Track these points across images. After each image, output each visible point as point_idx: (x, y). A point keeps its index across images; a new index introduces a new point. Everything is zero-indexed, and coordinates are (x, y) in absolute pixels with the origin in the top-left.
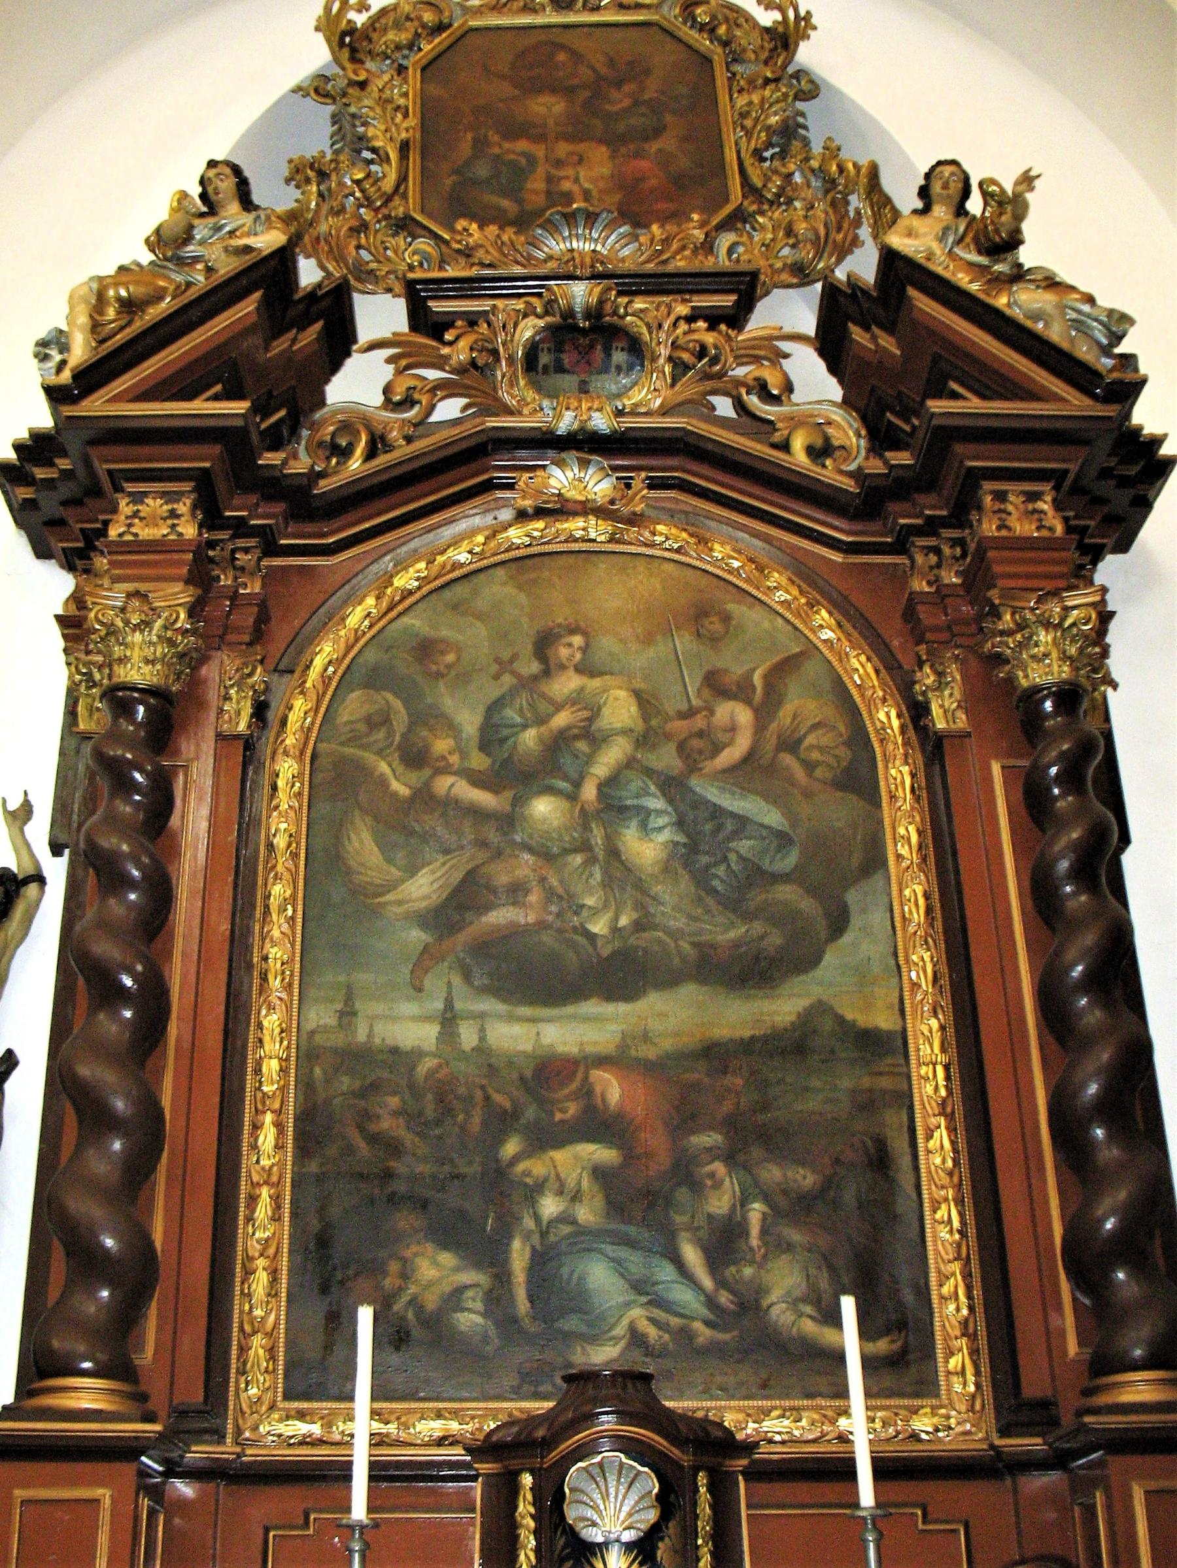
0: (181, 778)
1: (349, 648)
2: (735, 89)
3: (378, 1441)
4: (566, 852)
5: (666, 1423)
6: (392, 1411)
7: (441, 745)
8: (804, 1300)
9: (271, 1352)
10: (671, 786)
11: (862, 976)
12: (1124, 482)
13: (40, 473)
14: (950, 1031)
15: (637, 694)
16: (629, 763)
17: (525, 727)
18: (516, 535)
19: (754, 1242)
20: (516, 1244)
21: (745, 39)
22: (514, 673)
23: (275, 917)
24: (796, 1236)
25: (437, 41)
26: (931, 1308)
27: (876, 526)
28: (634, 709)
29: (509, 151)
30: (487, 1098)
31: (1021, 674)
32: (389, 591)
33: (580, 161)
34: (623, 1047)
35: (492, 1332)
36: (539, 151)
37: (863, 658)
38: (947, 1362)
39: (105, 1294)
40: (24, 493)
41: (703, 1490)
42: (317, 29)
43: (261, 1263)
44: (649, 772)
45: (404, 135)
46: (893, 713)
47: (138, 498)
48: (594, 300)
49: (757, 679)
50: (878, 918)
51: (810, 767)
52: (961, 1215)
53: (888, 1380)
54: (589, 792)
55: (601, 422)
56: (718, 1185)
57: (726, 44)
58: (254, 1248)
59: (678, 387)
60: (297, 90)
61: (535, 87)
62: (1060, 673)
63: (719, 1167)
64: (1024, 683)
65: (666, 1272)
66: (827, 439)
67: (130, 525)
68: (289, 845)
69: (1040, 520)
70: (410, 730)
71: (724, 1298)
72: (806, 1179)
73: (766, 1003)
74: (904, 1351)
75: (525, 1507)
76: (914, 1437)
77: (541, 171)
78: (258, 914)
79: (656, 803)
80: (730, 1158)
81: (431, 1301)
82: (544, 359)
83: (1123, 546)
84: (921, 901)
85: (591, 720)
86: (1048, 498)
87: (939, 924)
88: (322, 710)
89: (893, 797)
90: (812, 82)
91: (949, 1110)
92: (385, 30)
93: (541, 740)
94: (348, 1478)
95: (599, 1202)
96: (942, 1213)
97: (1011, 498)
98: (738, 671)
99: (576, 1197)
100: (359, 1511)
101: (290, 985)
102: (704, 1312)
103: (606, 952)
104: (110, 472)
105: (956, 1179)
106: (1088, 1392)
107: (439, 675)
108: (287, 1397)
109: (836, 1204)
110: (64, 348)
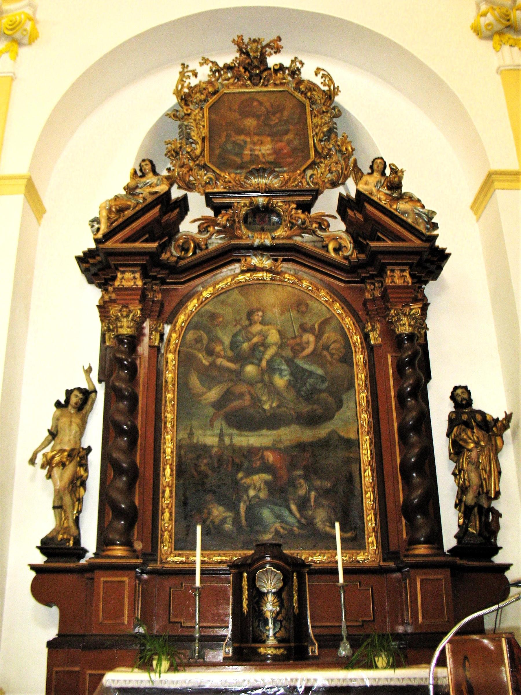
0: (139, 359)
1: (189, 316)
2: (313, 115)
3: (203, 562)
4: (257, 382)
5: (285, 558)
6: (206, 554)
7: (218, 348)
8: (327, 521)
9: (170, 537)
10: (290, 362)
11: (346, 422)
12: (433, 263)
13: (91, 261)
14: (373, 440)
15: (279, 332)
16: (276, 354)
17: (244, 342)
18: (241, 277)
19: (312, 504)
20: (242, 505)
21: (317, 96)
22: (241, 325)
23: (168, 404)
24: (324, 502)
25: (214, 98)
26: (364, 523)
27: (355, 275)
28: (278, 336)
29: (238, 139)
30: (233, 460)
31: (397, 330)
32: (201, 297)
33: (261, 143)
34: (274, 444)
35: (235, 530)
36: (248, 140)
37: (350, 319)
38: (368, 539)
39: (123, 522)
40: (85, 266)
41: (295, 578)
42: (174, 93)
43: (167, 510)
44: (282, 357)
45: (203, 135)
46: (358, 337)
47: (123, 272)
48: (266, 202)
49: (316, 326)
50: (352, 404)
51: (332, 355)
52: (374, 496)
53: (351, 544)
54: (264, 363)
55: (268, 242)
56: (302, 486)
57: (310, 99)
58: (165, 506)
59: (292, 230)
60: (167, 115)
61: (245, 114)
62: (409, 330)
63: (302, 481)
64: (398, 332)
65: (286, 513)
66: (340, 244)
67: (121, 282)
68: (172, 381)
69: (404, 279)
70: (208, 343)
71: (303, 521)
72: (328, 485)
73: (316, 430)
74: (356, 535)
75: (245, 583)
76: (358, 562)
77: (249, 146)
78: (163, 403)
79: (284, 367)
80: (306, 478)
81: (217, 521)
82: (250, 220)
83: (435, 278)
84: (365, 398)
85: (264, 340)
86: (408, 272)
87: (370, 406)
88: (181, 337)
89: (357, 365)
90: (339, 111)
91: (371, 464)
92: (196, 93)
93: (249, 347)
94: (195, 574)
95: (266, 492)
96: (368, 495)
97: (396, 272)
98: (310, 324)
99: (260, 490)
100: (198, 584)
101: (173, 425)
102: (297, 524)
103: (268, 414)
104: (115, 264)
105: (373, 484)
106: (407, 550)
107: (217, 325)
108: (176, 549)
109: (336, 492)
110: (99, 223)
